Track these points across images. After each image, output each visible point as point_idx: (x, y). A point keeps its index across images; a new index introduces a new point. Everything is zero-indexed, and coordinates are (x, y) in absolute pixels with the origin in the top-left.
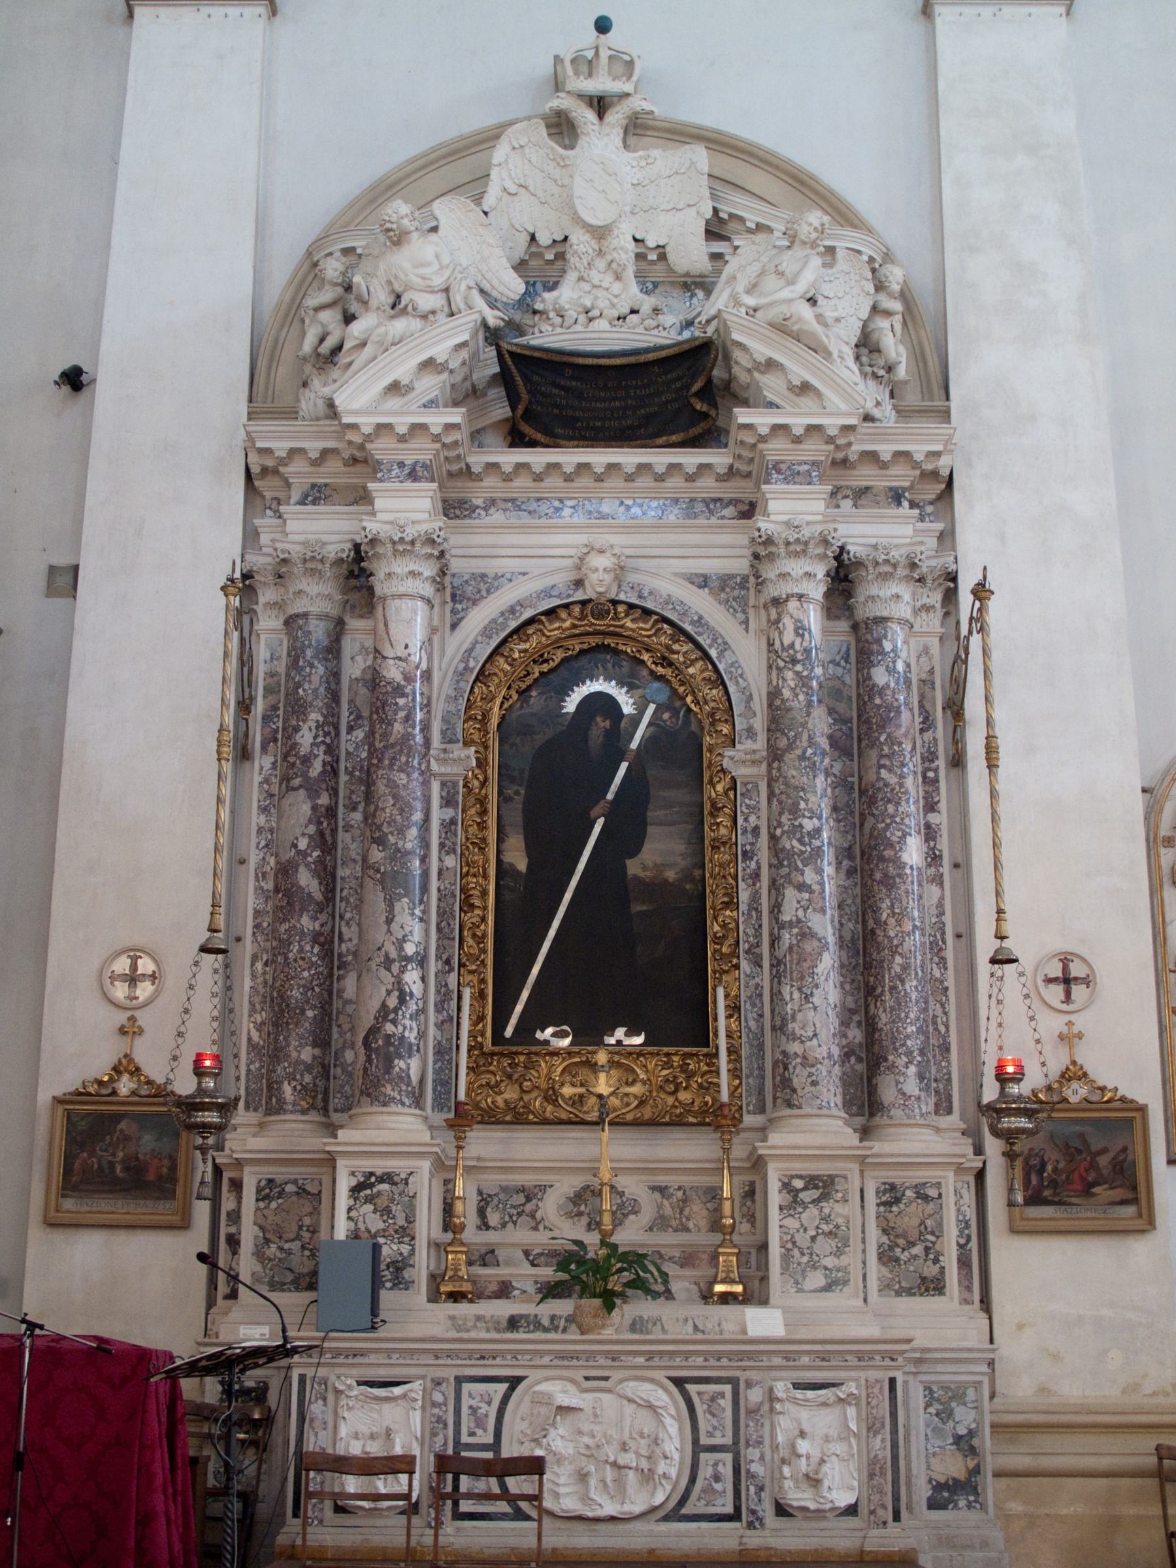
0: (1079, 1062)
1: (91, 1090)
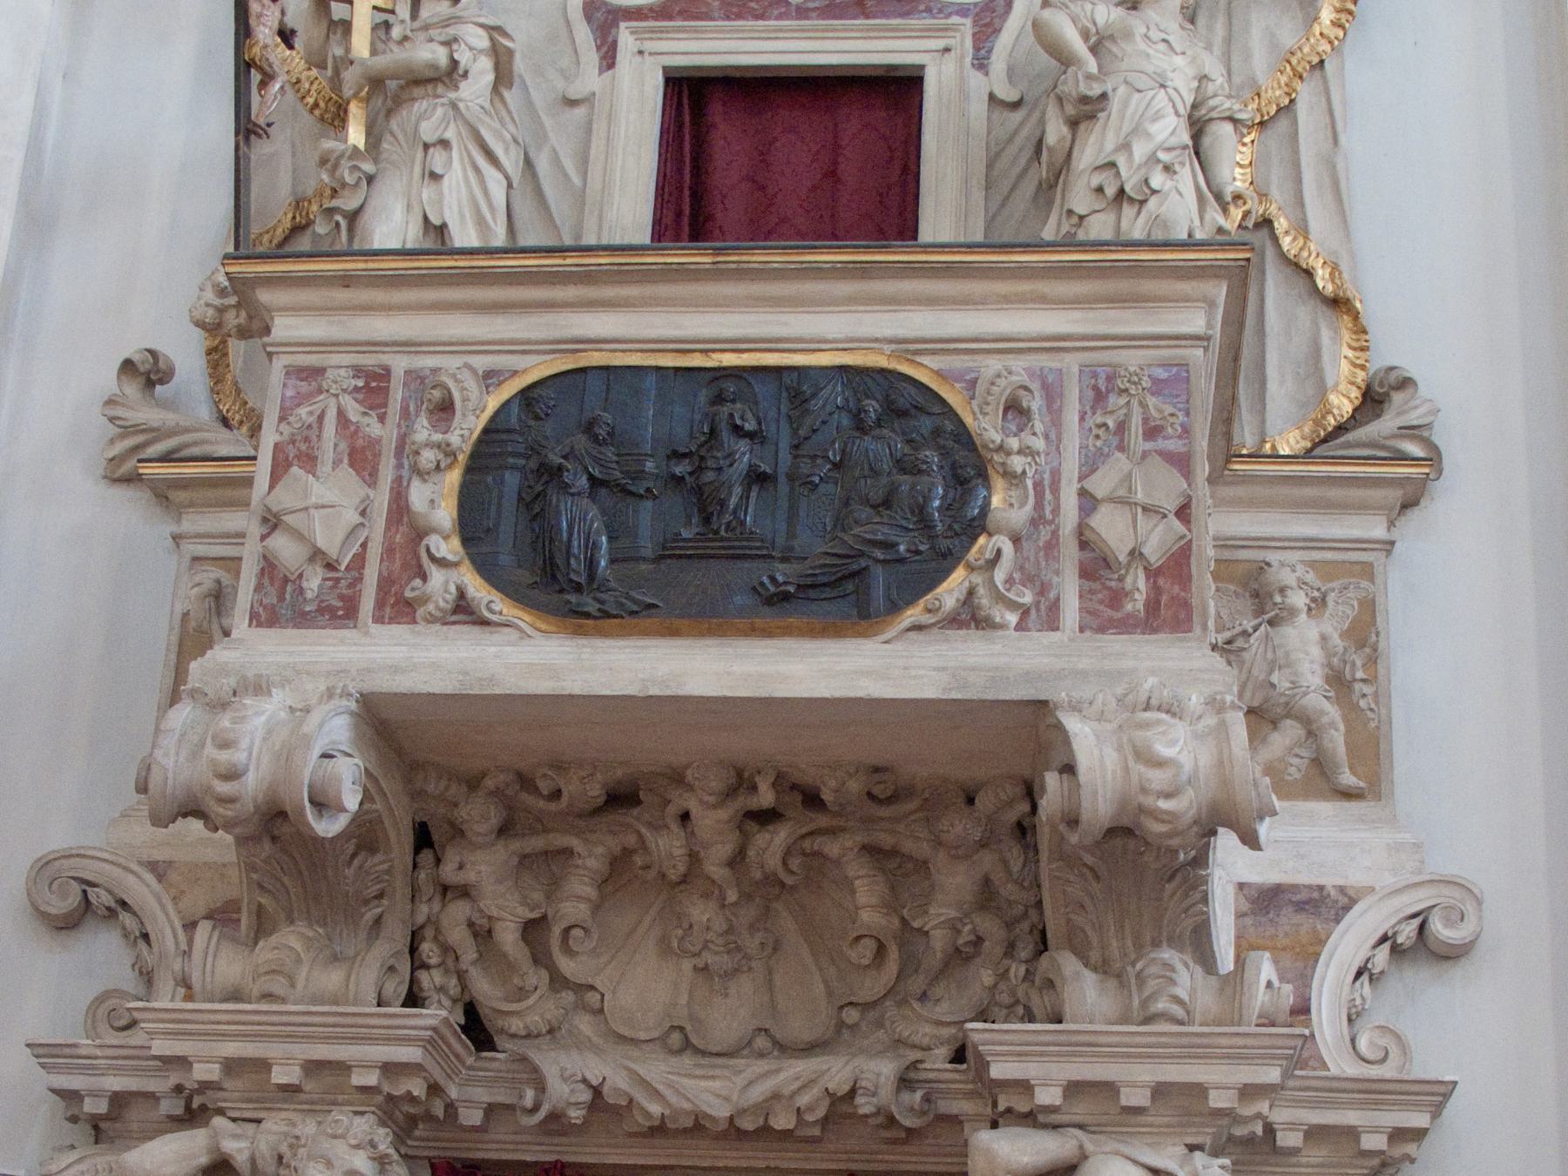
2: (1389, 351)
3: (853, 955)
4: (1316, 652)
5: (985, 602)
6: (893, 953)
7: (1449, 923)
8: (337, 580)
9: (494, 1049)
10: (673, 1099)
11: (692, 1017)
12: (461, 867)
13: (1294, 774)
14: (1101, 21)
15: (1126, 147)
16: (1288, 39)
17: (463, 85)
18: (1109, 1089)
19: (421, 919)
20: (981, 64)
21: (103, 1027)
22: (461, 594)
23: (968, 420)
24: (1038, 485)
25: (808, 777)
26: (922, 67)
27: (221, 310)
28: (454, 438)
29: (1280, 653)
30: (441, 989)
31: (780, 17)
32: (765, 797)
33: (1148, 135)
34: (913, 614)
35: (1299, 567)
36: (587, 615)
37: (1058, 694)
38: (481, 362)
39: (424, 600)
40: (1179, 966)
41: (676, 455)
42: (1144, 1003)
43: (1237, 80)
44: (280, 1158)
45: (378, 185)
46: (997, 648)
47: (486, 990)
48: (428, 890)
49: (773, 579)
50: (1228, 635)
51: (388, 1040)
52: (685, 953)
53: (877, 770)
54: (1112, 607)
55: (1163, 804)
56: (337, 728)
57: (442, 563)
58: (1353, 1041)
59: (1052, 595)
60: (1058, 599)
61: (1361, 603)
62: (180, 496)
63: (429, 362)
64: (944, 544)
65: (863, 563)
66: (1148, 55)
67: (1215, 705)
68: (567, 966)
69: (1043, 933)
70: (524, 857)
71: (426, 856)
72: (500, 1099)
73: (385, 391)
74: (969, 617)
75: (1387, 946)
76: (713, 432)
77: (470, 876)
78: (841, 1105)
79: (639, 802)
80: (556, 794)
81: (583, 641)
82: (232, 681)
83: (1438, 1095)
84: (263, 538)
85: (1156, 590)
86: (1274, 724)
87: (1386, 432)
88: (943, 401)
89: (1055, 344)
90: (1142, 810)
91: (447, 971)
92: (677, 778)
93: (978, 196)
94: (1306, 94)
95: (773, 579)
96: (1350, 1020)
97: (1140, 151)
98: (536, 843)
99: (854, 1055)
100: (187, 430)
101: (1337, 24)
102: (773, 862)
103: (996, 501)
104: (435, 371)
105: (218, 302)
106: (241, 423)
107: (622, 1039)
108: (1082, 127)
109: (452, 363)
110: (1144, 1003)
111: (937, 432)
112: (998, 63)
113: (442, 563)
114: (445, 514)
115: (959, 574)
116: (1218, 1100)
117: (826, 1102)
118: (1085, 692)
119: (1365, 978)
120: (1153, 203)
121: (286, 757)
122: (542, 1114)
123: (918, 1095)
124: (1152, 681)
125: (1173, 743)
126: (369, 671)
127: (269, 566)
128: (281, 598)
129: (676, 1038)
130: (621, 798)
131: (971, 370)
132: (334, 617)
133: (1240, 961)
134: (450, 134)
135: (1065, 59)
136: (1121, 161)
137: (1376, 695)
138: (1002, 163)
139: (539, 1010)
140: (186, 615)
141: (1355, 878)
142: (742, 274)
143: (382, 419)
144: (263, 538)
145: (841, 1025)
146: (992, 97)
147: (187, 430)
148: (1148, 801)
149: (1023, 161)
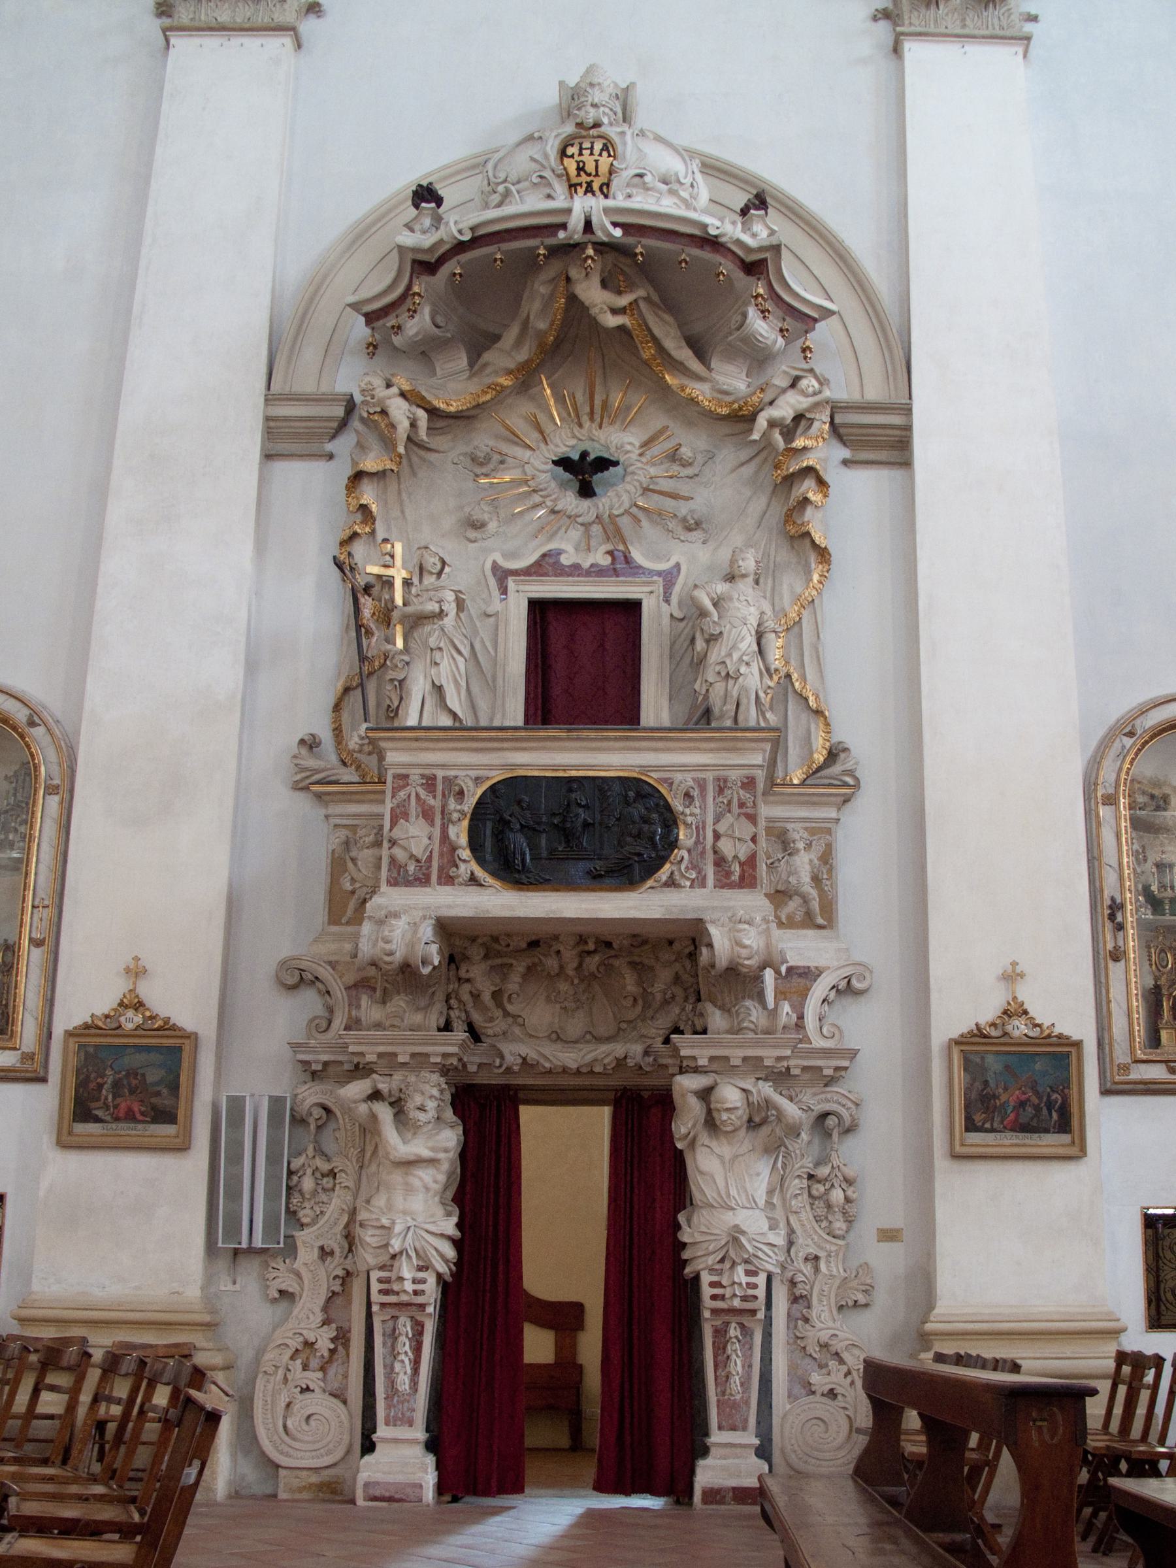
0: (1020, 999)
1: (100, 1024)
2: (841, 734)
3: (624, 1003)
4: (808, 867)
5: (677, 878)
6: (640, 1002)
7: (859, 981)
8: (421, 867)
9: (481, 1042)
10: (554, 1061)
11: (561, 1028)
12: (468, 971)
13: (798, 918)
14: (719, 592)
15: (730, 655)
16: (799, 590)
17: (445, 619)
18: (727, 1059)
19: (450, 990)
20: (667, 600)
21: (314, 1032)
22: (472, 873)
23: (669, 800)
24: (697, 828)
25: (609, 939)
26: (641, 599)
27: (362, 745)
28: (466, 809)
29: (793, 868)
30: (459, 1017)
31: (578, 576)
32: (591, 946)
33: (739, 649)
34: (650, 883)
35: (801, 831)
36: (523, 884)
37: (706, 917)
38: (473, 774)
39: (458, 876)
40: (752, 1008)
41: (554, 814)
42: (739, 1023)
43: (777, 608)
44: (401, 1090)
45: (411, 665)
46: (683, 895)
47: (477, 1018)
48: (453, 979)
49: (595, 868)
50: (771, 861)
51: (445, 1044)
52: (556, 1002)
53: (634, 936)
54: (726, 878)
55: (746, 962)
56: (427, 931)
57: (464, 861)
58: (821, 1028)
59: (703, 873)
60: (705, 875)
61: (826, 845)
62: (327, 798)
63: (452, 773)
64: (663, 853)
65: (630, 862)
66: (739, 609)
67: (765, 920)
68: (509, 1008)
69: (699, 992)
70: (492, 967)
71: (453, 966)
72: (485, 1061)
73: (434, 785)
74: (671, 883)
75: (835, 990)
76: (568, 805)
77: (471, 975)
78: (621, 1062)
79: (539, 946)
80: (508, 945)
81: (522, 893)
82: (383, 913)
83: (853, 1054)
84: (389, 849)
85: (743, 871)
86: (791, 897)
87: (837, 773)
88: (658, 791)
89: (704, 767)
90: (738, 964)
91: (460, 1010)
92: (556, 938)
93: (667, 662)
94: (806, 614)
95: (595, 868)
96: (820, 1020)
97: (735, 656)
98: (499, 961)
99: (626, 1043)
100: (327, 770)
101: (821, 582)
102: (593, 968)
103: (681, 837)
104: (456, 777)
105: (360, 742)
106: (351, 764)
107: (531, 1036)
108: (712, 643)
109: (461, 773)
110: (739, 1023)
111: (657, 805)
112: (674, 599)
113: (464, 861)
114: (463, 840)
115: (667, 866)
116: (767, 1063)
117: (615, 1062)
118: (716, 916)
119: (826, 1003)
120: (741, 679)
121: (412, 945)
122: (504, 1068)
123: (651, 1059)
124: (742, 912)
125: (749, 939)
126: (439, 907)
127: (393, 860)
128: (399, 874)
129: (554, 1036)
130: (534, 944)
131: (670, 779)
132: (421, 882)
133: (776, 1005)
134: (442, 645)
135: (703, 614)
136: (728, 662)
137: (832, 884)
138: (677, 647)
139: (500, 1025)
140: (333, 851)
141: (822, 963)
142: (578, 739)
143: (434, 797)
144: (389, 849)
145: (619, 1029)
146: (671, 615)
147: (327, 770)
148: (741, 961)
149: (685, 645)
